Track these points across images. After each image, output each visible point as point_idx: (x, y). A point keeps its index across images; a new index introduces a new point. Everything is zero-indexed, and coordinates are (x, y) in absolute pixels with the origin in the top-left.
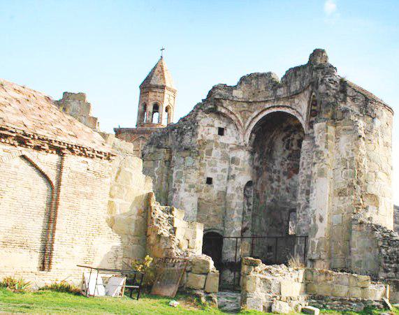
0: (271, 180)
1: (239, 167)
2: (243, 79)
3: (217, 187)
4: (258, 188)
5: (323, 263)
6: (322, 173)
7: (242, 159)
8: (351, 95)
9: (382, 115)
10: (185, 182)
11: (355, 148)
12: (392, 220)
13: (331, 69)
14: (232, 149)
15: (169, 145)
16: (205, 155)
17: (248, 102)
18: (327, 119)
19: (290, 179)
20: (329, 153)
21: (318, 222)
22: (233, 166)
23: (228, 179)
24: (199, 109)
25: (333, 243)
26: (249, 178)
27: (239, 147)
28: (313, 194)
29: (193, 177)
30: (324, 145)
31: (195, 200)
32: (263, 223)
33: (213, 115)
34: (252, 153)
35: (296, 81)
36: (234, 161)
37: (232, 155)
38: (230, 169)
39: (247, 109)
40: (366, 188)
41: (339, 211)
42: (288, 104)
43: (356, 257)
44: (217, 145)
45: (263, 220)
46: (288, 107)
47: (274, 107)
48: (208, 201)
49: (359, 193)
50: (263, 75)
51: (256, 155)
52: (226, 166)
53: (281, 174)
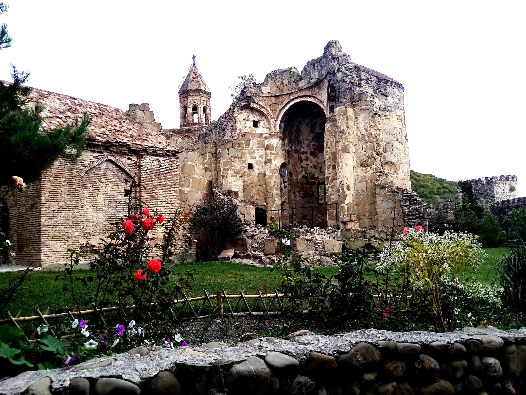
0: (301, 160)
1: (274, 152)
2: (268, 76)
3: (257, 170)
4: (290, 167)
6: (345, 150)
7: (275, 145)
8: (365, 78)
10: (231, 170)
11: (373, 124)
13: (345, 57)
15: (214, 140)
16: (244, 146)
17: (275, 96)
18: (345, 103)
19: (316, 158)
20: (350, 131)
22: (269, 152)
25: (360, 207)
26: (283, 161)
27: (272, 136)
29: (237, 165)
30: (345, 125)
31: (240, 183)
33: (248, 111)
34: (283, 139)
37: (266, 143)
38: (266, 155)
39: (274, 102)
41: (363, 179)
42: (309, 93)
44: (253, 137)
45: (297, 194)
46: (310, 96)
47: (297, 98)
51: (286, 141)
52: (262, 152)
53: (308, 155)
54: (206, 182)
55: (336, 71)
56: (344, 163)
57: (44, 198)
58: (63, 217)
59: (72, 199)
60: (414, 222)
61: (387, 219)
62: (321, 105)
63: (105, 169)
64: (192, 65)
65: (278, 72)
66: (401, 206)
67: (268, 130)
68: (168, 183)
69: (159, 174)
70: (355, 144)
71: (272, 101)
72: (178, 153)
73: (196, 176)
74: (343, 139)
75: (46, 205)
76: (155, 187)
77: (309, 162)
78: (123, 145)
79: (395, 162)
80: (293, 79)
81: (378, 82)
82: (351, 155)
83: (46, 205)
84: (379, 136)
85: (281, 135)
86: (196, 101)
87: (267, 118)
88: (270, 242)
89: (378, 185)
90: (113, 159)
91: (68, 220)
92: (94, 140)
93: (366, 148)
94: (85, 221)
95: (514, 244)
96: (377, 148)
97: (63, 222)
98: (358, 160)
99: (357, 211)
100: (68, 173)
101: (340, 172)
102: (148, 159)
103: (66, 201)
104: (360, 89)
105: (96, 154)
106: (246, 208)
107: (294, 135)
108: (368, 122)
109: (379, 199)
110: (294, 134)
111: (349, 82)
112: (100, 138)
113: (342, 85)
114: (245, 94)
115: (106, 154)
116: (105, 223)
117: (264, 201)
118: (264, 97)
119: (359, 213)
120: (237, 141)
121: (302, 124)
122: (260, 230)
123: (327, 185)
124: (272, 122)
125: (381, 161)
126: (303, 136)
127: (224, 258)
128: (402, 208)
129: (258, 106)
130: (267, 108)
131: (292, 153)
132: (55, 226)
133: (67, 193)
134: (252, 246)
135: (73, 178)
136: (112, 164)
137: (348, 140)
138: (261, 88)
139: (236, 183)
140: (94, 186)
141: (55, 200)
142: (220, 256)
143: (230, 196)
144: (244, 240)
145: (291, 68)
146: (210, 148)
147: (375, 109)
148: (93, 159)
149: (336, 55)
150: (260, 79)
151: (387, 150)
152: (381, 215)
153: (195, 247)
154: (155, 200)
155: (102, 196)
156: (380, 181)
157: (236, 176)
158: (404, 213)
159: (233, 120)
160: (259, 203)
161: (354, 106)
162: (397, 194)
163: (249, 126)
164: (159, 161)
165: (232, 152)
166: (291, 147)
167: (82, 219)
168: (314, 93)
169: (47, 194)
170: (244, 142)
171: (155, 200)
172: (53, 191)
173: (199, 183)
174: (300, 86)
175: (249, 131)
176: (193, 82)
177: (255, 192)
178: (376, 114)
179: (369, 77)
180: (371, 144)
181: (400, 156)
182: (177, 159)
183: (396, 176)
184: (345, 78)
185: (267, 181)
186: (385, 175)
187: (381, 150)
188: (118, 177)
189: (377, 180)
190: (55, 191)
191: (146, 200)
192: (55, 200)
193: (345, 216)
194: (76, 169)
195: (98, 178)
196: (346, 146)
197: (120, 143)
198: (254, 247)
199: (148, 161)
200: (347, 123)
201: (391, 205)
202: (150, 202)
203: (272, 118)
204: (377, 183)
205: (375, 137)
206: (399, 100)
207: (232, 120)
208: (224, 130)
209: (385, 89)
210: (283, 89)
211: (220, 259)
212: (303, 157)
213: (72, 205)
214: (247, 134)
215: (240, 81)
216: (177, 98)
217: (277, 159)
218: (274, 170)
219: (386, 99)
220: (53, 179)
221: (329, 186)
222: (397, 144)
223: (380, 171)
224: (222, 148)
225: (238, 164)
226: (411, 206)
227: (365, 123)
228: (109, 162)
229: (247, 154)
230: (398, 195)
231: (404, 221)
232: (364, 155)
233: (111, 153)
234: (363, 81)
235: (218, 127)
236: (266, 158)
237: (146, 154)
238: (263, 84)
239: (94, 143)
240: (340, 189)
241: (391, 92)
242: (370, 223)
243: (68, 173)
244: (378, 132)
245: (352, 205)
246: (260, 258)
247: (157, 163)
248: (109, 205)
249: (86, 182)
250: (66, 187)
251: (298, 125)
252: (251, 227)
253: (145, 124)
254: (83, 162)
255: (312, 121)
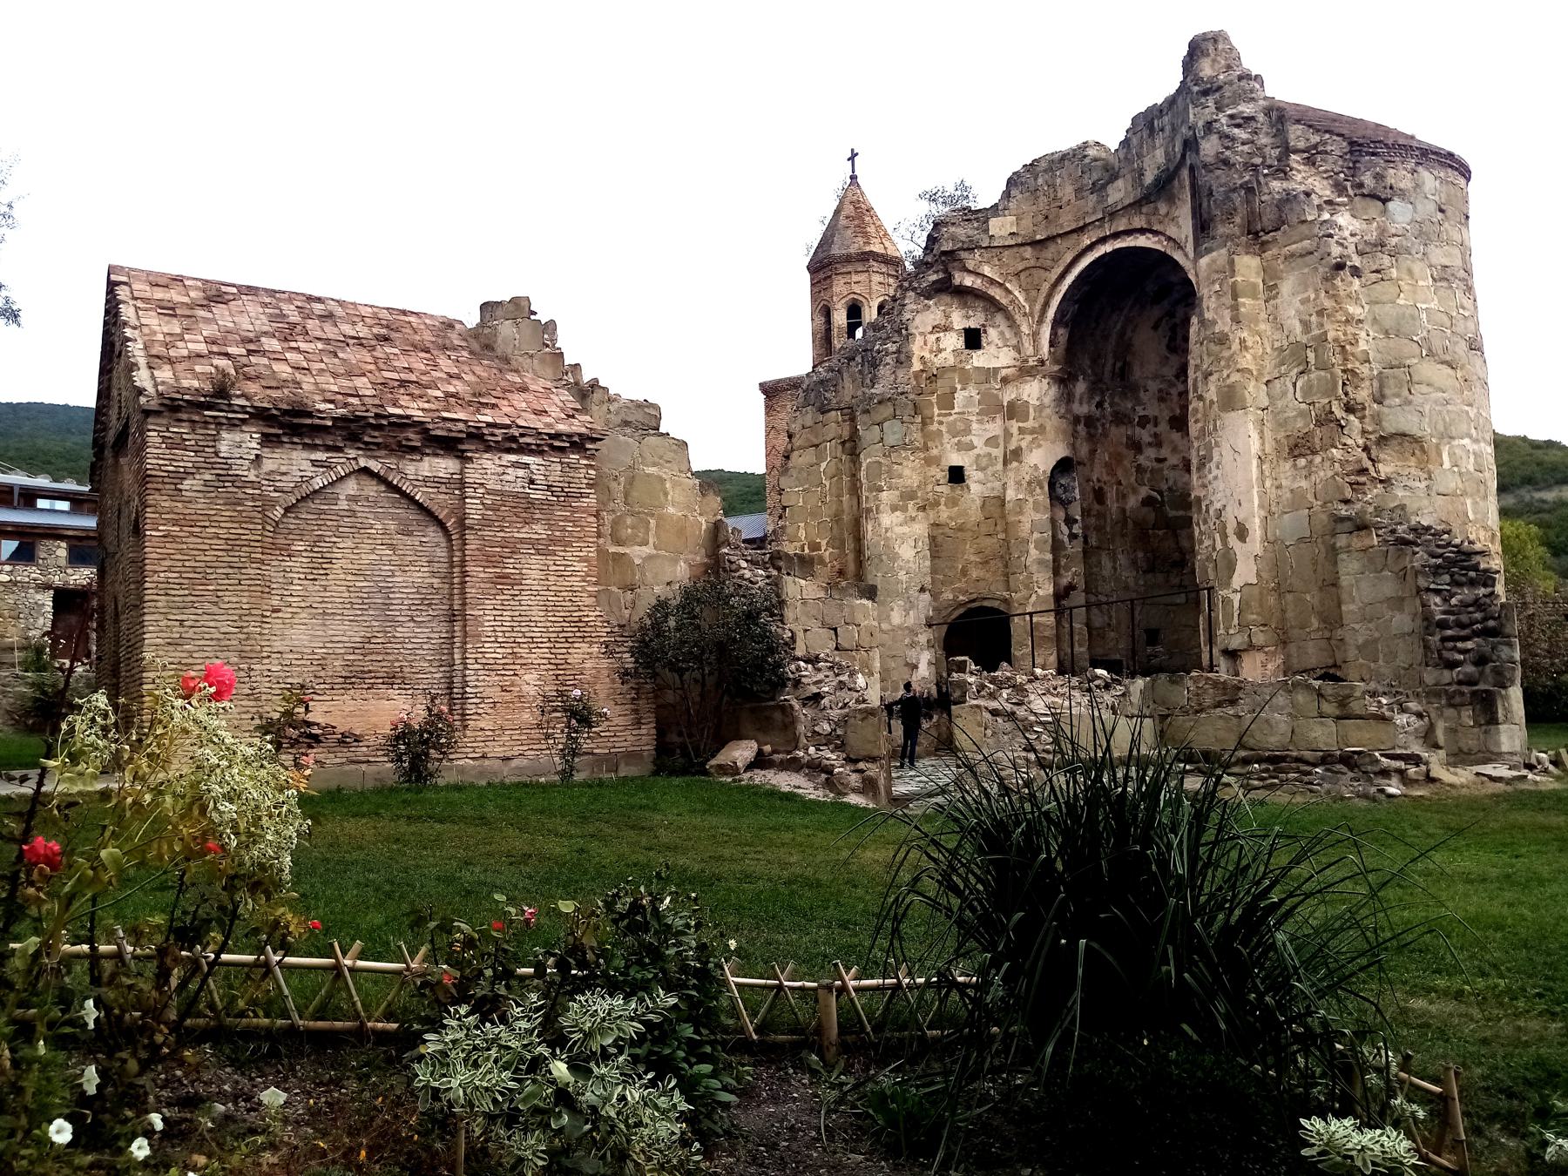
0: (1136, 447)
1: (1030, 424)
2: (1011, 182)
3: (976, 487)
4: (1098, 473)
5: (1260, 657)
6: (1231, 400)
7: (1034, 402)
8: (1301, 145)
9: (1417, 186)
10: (890, 488)
11: (1328, 304)
12: (1492, 506)
13: (1243, 83)
14: (1005, 381)
15: (848, 399)
16: (936, 411)
17: (1034, 244)
18: (1229, 237)
20: (1245, 334)
21: (1233, 541)
22: (1014, 426)
23: (1005, 463)
24: (907, 289)
25: (1289, 597)
26: (1061, 451)
27: (1025, 372)
28: (1213, 465)
29: (910, 472)
30: (1227, 314)
31: (920, 529)
32: (1119, 568)
33: (946, 298)
34: (1064, 380)
35: (1154, 147)
36: (1014, 411)
37: (1008, 395)
38: (1008, 434)
39: (1032, 263)
40: (1378, 420)
41: (1297, 496)
42: (1139, 222)
43: (1357, 633)
44: (965, 379)
45: (1122, 559)
46: (1142, 231)
48: (960, 529)
49: (1355, 439)
50: (1063, 158)
51: (1081, 387)
52: (995, 428)
53: (1163, 427)
54: (704, 527)
55: (1199, 134)
56: (1225, 449)
57: (154, 585)
58: (212, 639)
59: (240, 587)
60: (1465, 651)
61: (1376, 641)
62: (1178, 256)
63: (352, 499)
64: (849, 181)
65: (1043, 164)
66: (1419, 590)
67: (1013, 354)
68: (558, 533)
69: (525, 508)
70: (1265, 380)
71: (1023, 259)
72: (594, 440)
73: (671, 510)
74: (1223, 363)
75: (159, 604)
76: (513, 547)
77: (1165, 452)
78: (405, 423)
79: (1419, 434)
80: (1088, 181)
81: (1351, 152)
82: (1251, 417)
83: (159, 604)
84: (1353, 344)
85: (1056, 368)
86: (856, 288)
87: (1009, 318)
88: (862, 720)
89: (1342, 520)
90: (375, 466)
91: (227, 648)
92: (310, 415)
93: (1308, 390)
94: (288, 649)
95: (1401, 772)
96: (1349, 389)
97: (211, 655)
98: (1281, 435)
99: (1278, 614)
100: (228, 514)
101: (1216, 478)
102: (488, 464)
103: (220, 594)
104: (1285, 185)
105: (320, 456)
106: (841, 609)
107: (1108, 368)
108: (1313, 296)
109: (1349, 568)
110: (1110, 361)
111: (1245, 164)
112: (332, 406)
113: (1218, 177)
114: (936, 247)
115: (352, 453)
116: (351, 657)
117: (1001, 586)
118: (998, 251)
119: (1283, 620)
120: (912, 396)
121: (1136, 326)
122: (841, 678)
123: (1198, 525)
124: (1025, 329)
125: (1364, 432)
126: (1142, 365)
127: (723, 770)
128: (1421, 598)
129: (979, 281)
130: (1008, 285)
131: (1103, 425)
132: (186, 664)
133: (225, 571)
134: (815, 732)
135: (244, 525)
136: (374, 482)
137: (1239, 366)
138: (986, 222)
139: (906, 529)
140: (316, 549)
141: (187, 592)
142: (713, 762)
143: (779, 569)
144: (786, 709)
145: (1085, 145)
146: (835, 425)
147: (1336, 251)
148: (309, 470)
149: (1212, 79)
150: (987, 194)
151: (1387, 392)
152: (1357, 627)
153: (654, 731)
154: (513, 585)
155: (342, 576)
156: (1358, 506)
157: (904, 509)
158: (1427, 617)
159: (902, 332)
160: (985, 593)
161: (1264, 246)
162: (1408, 550)
163: (949, 350)
164: (526, 466)
165: (893, 430)
166: (1099, 405)
167: (275, 644)
168: (1153, 219)
169: (162, 575)
170: (934, 399)
171: (513, 585)
172: (180, 564)
173: (681, 531)
174: (1110, 201)
175: (951, 361)
176: (849, 232)
177: (973, 558)
178: (1340, 267)
179: (1315, 139)
180: (1322, 373)
181: (1440, 412)
182: (587, 458)
183: (1426, 483)
184: (1228, 153)
185: (1012, 519)
186: (1381, 481)
187: (1362, 395)
188: (393, 519)
189: (1347, 502)
190: (187, 564)
191: (482, 585)
192: (187, 592)
193: (1231, 632)
194: (254, 500)
195: (329, 523)
196: (1231, 387)
197: (393, 420)
198: (819, 734)
199: (489, 469)
200: (1235, 308)
201: (1389, 588)
202: (494, 592)
203: (1025, 314)
204: (1344, 511)
205: (1338, 350)
206: (1442, 211)
207: (899, 332)
208: (874, 365)
209: (1379, 177)
210: (1058, 217)
211: (712, 770)
212: (1145, 435)
213: (238, 606)
214: (944, 372)
215: (925, 207)
216: (803, 281)
217: (1040, 446)
218: (1029, 483)
219: (1385, 212)
220: (181, 531)
221: (1203, 528)
222: (1429, 370)
223: (1357, 467)
224: (865, 424)
225: (913, 469)
226: (1455, 590)
227: (1303, 302)
228: (364, 477)
229: (946, 437)
230: (1415, 553)
231: (1426, 647)
232: (1301, 414)
233: (369, 448)
234: (1293, 156)
235: (859, 359)
236: (1006, 448)
237: (481, 447)
238: (995, 210)
239: (309, 421)
240: (1217, 536)
241: (1402, 185)
242: (1325, 653)
243: (228, 514)
244: (1350, 330)
245: (1256, 591)
246: (828, 770)
247: (521, 473)
248: (363, 603)
249: (291, 537)
250: (220, 553)
251: (1122, 334)
252: (819, 670)
253: (520, 359)
254: (278, 478)
255: (1171, 314)
